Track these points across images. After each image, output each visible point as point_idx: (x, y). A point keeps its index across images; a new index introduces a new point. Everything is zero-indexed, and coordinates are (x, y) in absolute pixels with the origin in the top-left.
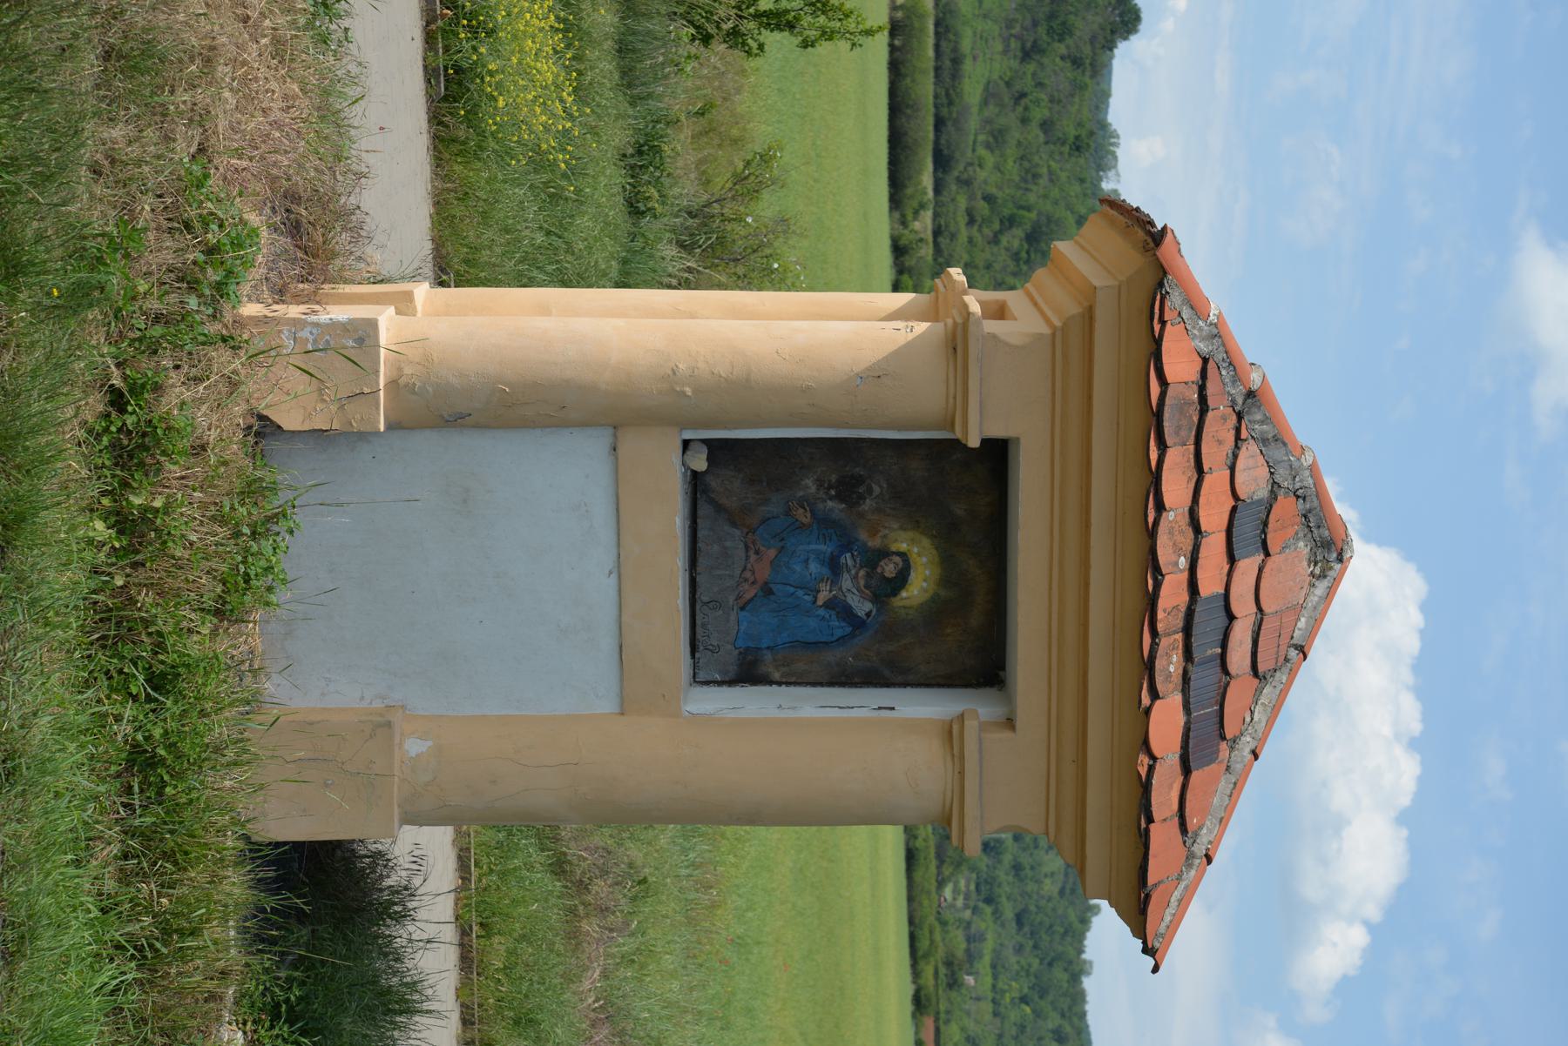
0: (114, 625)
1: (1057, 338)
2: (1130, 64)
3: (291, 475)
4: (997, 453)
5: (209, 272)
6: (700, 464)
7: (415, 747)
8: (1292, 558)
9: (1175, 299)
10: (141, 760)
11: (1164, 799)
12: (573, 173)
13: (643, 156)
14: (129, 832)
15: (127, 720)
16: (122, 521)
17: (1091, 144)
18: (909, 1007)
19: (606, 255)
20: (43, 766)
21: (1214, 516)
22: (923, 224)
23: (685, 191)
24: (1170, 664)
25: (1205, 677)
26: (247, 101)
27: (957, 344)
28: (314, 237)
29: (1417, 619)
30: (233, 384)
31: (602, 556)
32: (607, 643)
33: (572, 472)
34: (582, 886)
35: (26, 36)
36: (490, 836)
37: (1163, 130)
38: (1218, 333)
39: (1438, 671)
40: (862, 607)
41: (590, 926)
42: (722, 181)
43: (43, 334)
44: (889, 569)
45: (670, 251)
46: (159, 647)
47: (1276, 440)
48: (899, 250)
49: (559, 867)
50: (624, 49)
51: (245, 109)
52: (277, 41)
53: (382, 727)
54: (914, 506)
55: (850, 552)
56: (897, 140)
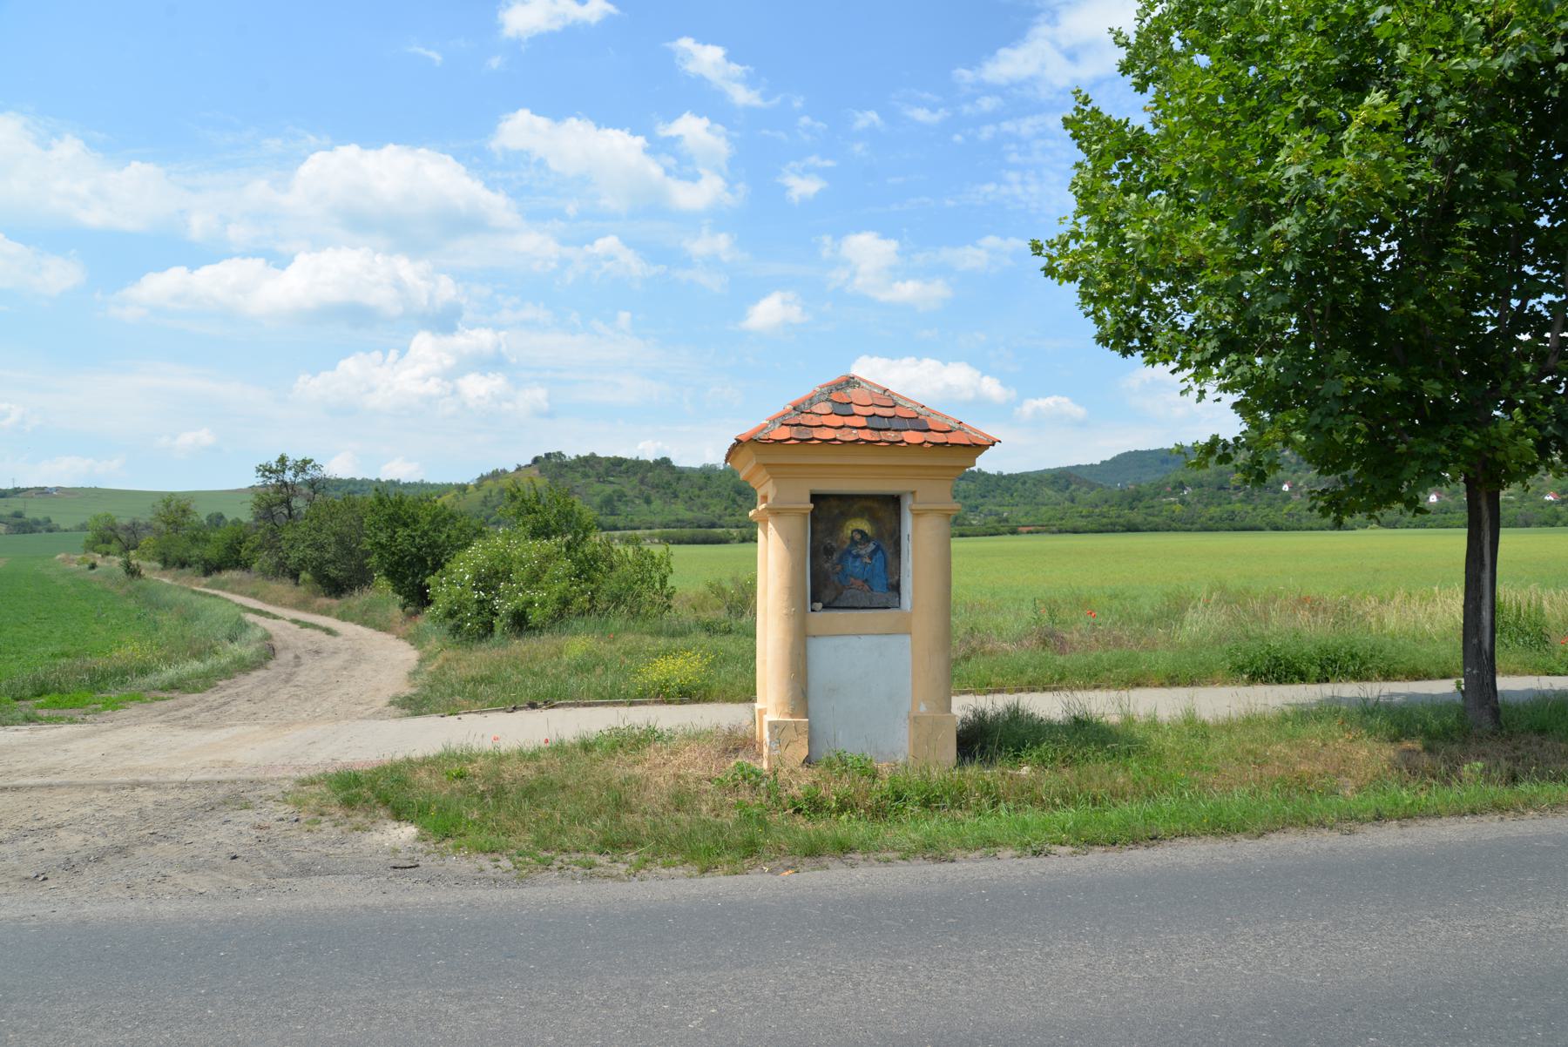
0: (878, 813)
1: (773, 476)
2: (679, 461)
3: (824, 753)
4: (816, 498)
5: (752, 779)
6: (820, 605)
7: (923, 708)
8: (852, 394)
9: (761, 435)
10: (926, 803)
11: (940, 438)
12: (716, 652)
13: (709, 628)
14: (952, 806)
15: (913, 808)
16: (842, 809)
17: (707, 473)
18: (1015, 537)
19: (745, 644)
20: (928, 835)
21: (839, 421)
22: (734, 532)
23: (723, 614)
24: (891, 436)
25: (896, 424)
26: (692, 764)
27: (776, 512)
28: (738, 743)
29: (875, 359)
30: (792, 771)
31: (854, 641)
32: (885, 639)
33: (825, 653)
34: (974, 651)
35: (672, 836)
36: (955, 683)
37: (701, 448)
38: (773, 421)
39: (893, 352)
40: (872, 546)
41: (988, 647)
42: (718, 602)
43: (775, 835)
44: (858, 537)
45: (744, 620)
46: (886, 797)
47: (811, 400)
48: (744, 540)
49: (967, 658)
50: (673, 635)
51: (696, 766)
52: (672, 753)
53: (916, 720)
54: (834, 526)
55: (851, 554)
56: (706, 541)
